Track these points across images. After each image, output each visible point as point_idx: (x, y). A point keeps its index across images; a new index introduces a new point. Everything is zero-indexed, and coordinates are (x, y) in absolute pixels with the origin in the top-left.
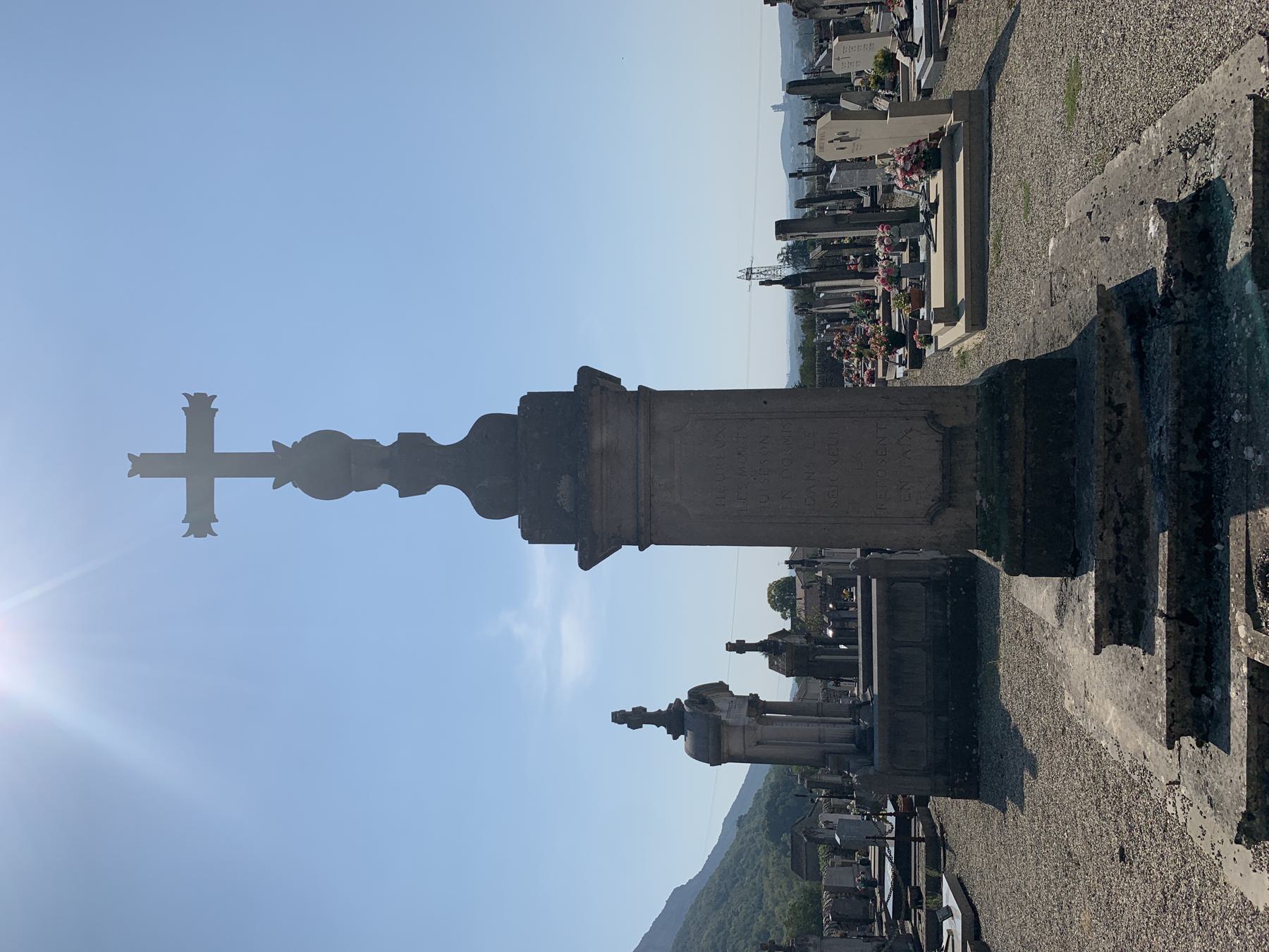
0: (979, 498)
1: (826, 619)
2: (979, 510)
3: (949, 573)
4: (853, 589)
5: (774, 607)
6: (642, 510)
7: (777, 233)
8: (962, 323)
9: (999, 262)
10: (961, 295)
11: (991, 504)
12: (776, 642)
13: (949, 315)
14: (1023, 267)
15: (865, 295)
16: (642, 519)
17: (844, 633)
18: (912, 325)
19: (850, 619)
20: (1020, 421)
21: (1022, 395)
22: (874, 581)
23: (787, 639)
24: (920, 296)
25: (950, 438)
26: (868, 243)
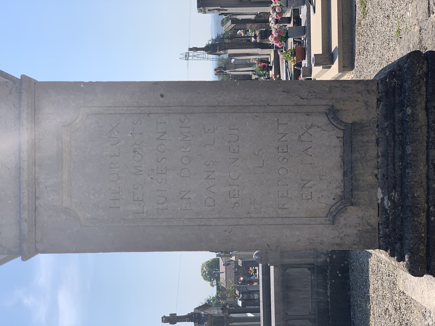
0: (380, 195)
1: (237, 292)
2: (381, 208)
3: (328, 260)
4: (257, 268)
5: (205, 278)
6: (25, 215)
7: (199, 6)
8: (336, 66)
9: (365, 14)
10: (335, 43)
11: (393, 202)
12: (199, 314)
13: (326, 59)
14: (387, 13)
15: (262, 61)
16: (25, 225)
17: (250, 303)
18: (297, 73)
19: (254, 291)
20: (422, 115)
21: (424, 88)
22: (272, 268)
23: (208, 311)
24: (302, 51)
25: (351, 133)
26: (262, 20)
